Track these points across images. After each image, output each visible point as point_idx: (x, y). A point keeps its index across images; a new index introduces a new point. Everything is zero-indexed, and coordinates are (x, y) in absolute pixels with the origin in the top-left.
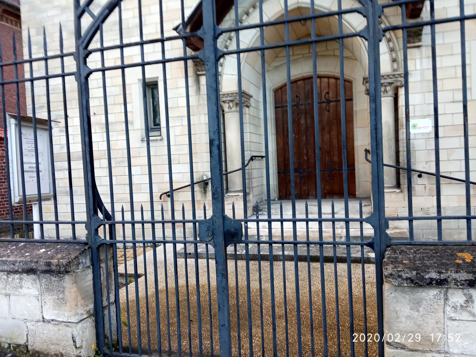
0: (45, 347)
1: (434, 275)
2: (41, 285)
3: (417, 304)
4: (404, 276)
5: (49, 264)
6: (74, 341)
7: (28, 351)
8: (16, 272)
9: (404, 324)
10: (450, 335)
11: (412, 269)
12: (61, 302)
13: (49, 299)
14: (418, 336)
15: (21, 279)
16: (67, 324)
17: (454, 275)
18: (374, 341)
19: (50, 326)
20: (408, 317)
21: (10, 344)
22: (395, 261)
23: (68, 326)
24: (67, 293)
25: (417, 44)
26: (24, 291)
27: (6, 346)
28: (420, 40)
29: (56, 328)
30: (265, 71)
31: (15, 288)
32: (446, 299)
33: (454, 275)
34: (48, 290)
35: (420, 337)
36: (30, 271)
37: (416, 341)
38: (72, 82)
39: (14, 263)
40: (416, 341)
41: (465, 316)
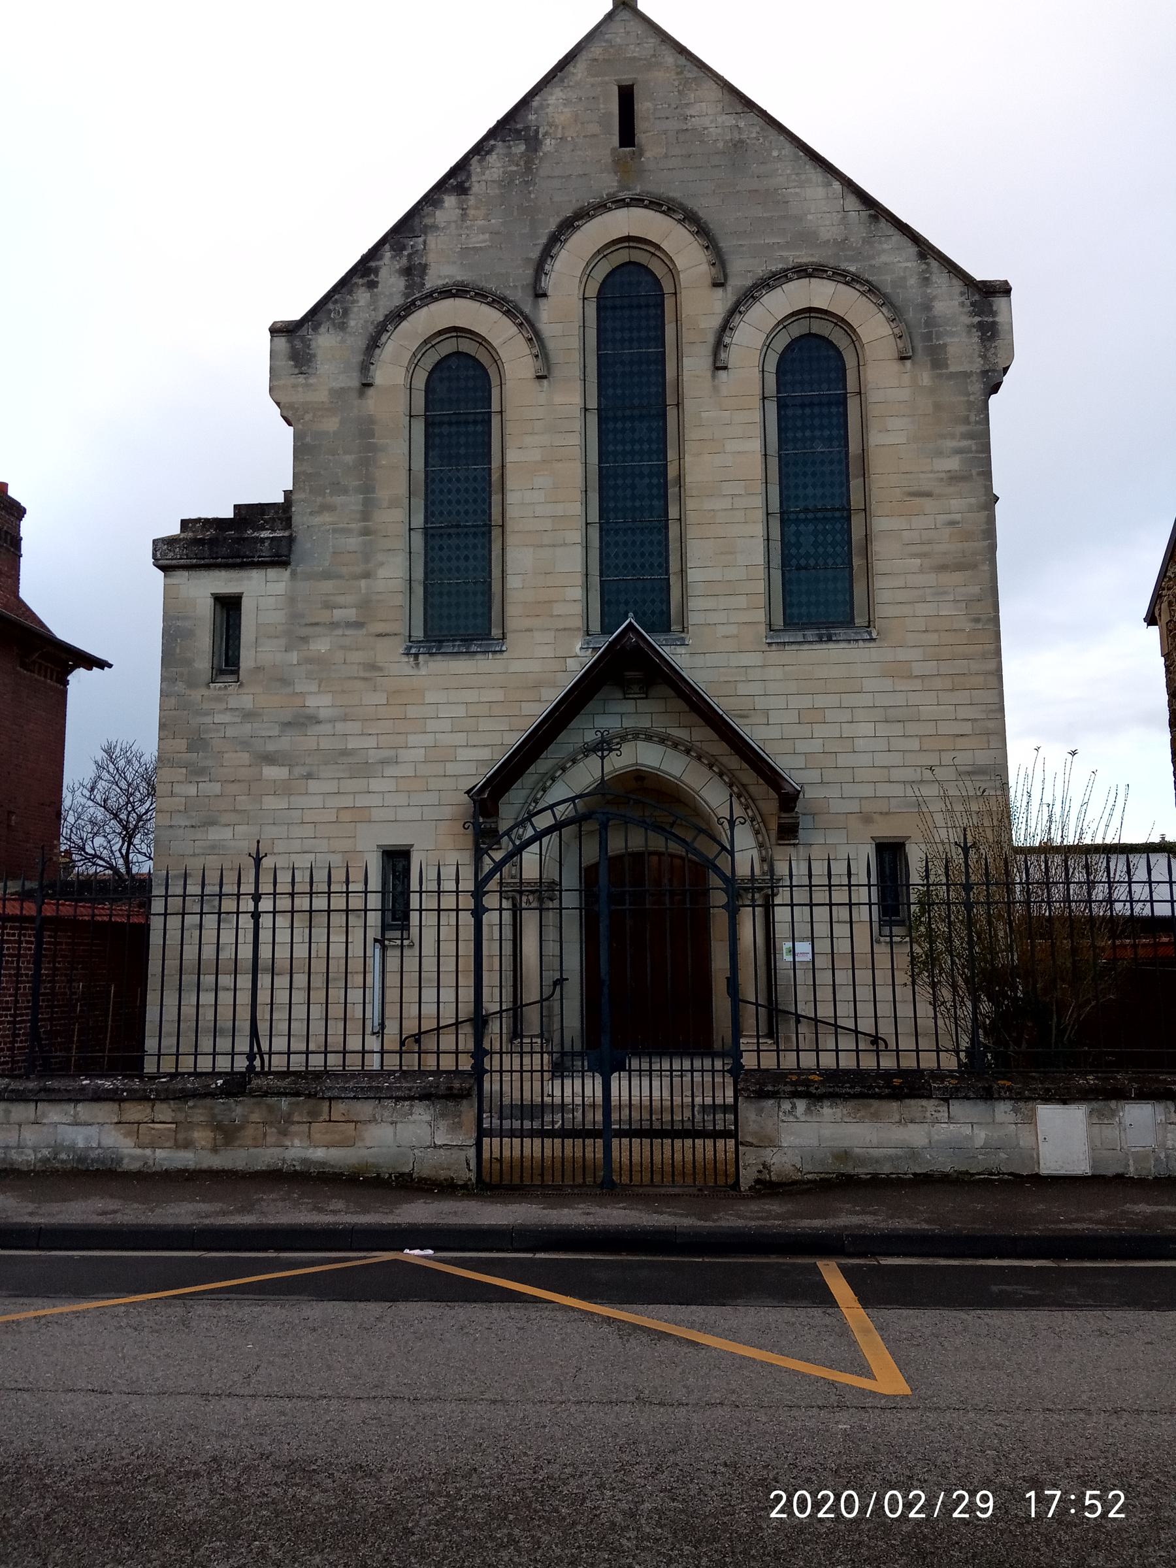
0: (434, 1173)
1: (770, 1088)
2: (435, 1111)
3: (760, 1111)
4: (751, 1089)
5: (451, 1088)
6: (468, 1164)
7: (413, 1180)
8: (405, 1099)
9: (753, 1127)
10: (1092, 1497)
11: (755, 1084)
12: (455, 1128)
13: (443, 1124)
14: (985, 1499)
15: (412, 1106)
16: (460, 1147)
17: (783, 1088)
18: (839, 1516)
19: (442, 1151)
20: (754, 1121)
21: (390, 1175)
22: (746, 1081)
23: (462, 1150)
24: (464, 1117)
25: (792, 842)
26: (415, 1117)
27: (387, 1176)
28: (796, 837)
29: (448, 1153)
30: (490, 625)
31: (405, 1115)
32: (779, 1107)
33: (783, 1088)
34: (443, 1116)
35: (991, 1504)
36: (421, 1098)
37: (978, 1513)
38: (467, 919)
39: (410, 1089)
40: (978, 1513)
41: (791, 1119)
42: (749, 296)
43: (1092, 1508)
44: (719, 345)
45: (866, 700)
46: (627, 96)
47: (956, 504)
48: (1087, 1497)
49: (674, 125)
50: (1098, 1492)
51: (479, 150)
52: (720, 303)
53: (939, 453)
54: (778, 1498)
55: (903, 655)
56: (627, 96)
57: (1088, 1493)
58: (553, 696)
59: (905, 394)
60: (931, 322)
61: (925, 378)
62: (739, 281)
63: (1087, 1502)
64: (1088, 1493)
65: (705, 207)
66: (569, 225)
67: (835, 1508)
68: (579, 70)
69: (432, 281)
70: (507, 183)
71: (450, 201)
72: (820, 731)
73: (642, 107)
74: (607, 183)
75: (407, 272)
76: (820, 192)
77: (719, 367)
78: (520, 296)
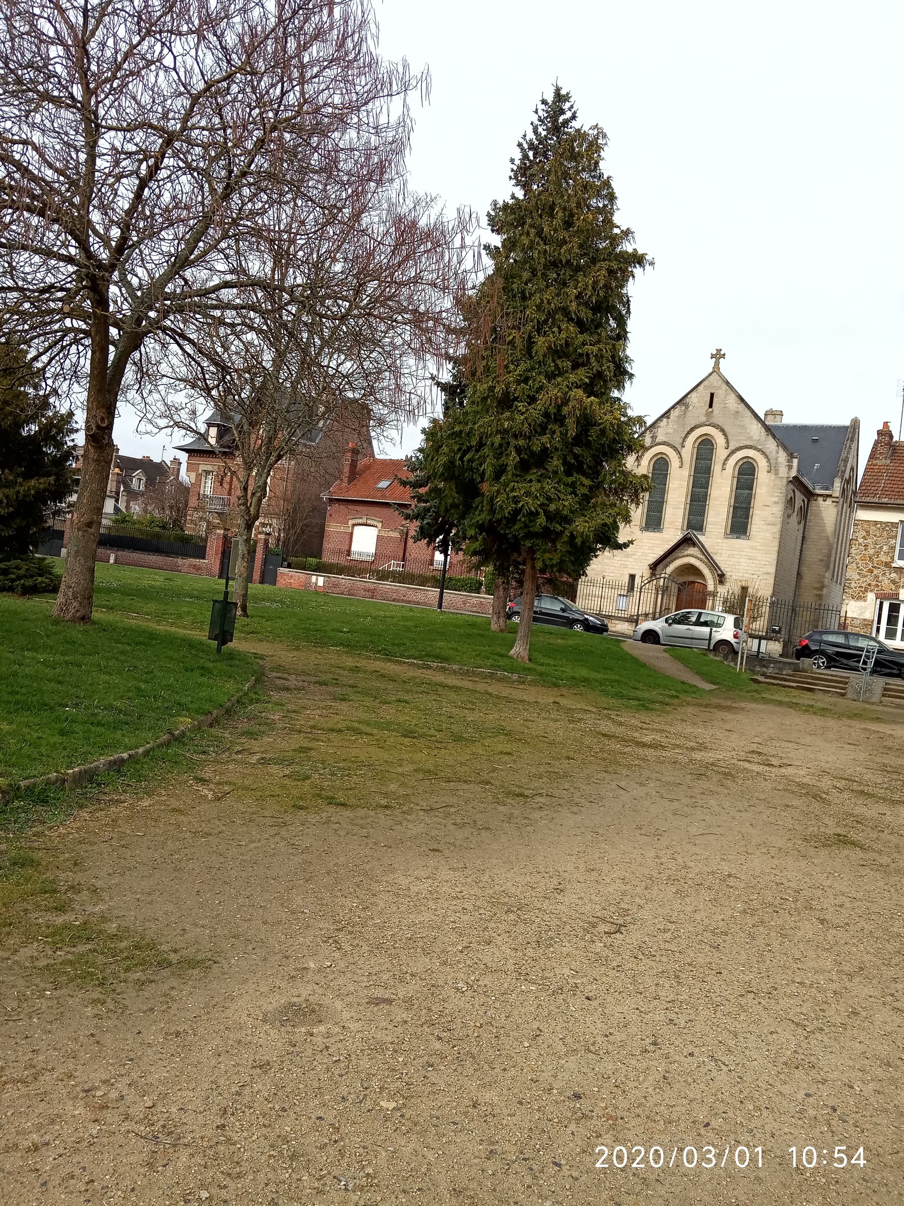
42: (733, 452)
43: (841, 1160)
44: (724, 464)
45: (745, 554)
46: (712, 395)
47: (775, 509)
48: (836, 1151)
49: (722, 405)
50: (844, 1148)
51: (673, 407)
52: (727, 452)
53: (773, 496)
54: (601, 1153)
55: (756, 544)
56: (712, 395)
57: (837, 1148)
58: (672, 544)
59: (767, 481)
60: (776, 463)
61: (773, 477)
62: (732, 448)
63: (836, 1156)
64: (837, 1148)
65: (726, 428)
66: (692, 430)
67: (645, 1160)
68: (701, 388)
69: (658, 440)
70: (679, 417)
71: (665, 420)
72: (733, 559)
73: (715, 400)
74: (703, 419)
75: (652, 437)
76: (755, 427)
77: (724, 469)
78: (678, 447)
